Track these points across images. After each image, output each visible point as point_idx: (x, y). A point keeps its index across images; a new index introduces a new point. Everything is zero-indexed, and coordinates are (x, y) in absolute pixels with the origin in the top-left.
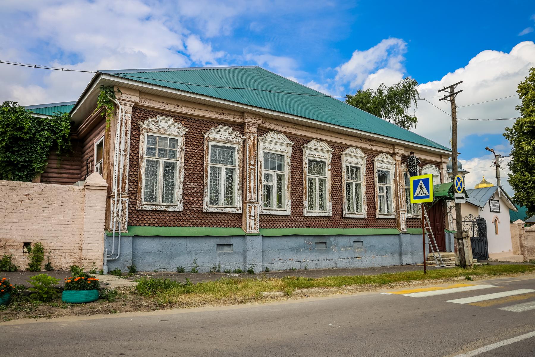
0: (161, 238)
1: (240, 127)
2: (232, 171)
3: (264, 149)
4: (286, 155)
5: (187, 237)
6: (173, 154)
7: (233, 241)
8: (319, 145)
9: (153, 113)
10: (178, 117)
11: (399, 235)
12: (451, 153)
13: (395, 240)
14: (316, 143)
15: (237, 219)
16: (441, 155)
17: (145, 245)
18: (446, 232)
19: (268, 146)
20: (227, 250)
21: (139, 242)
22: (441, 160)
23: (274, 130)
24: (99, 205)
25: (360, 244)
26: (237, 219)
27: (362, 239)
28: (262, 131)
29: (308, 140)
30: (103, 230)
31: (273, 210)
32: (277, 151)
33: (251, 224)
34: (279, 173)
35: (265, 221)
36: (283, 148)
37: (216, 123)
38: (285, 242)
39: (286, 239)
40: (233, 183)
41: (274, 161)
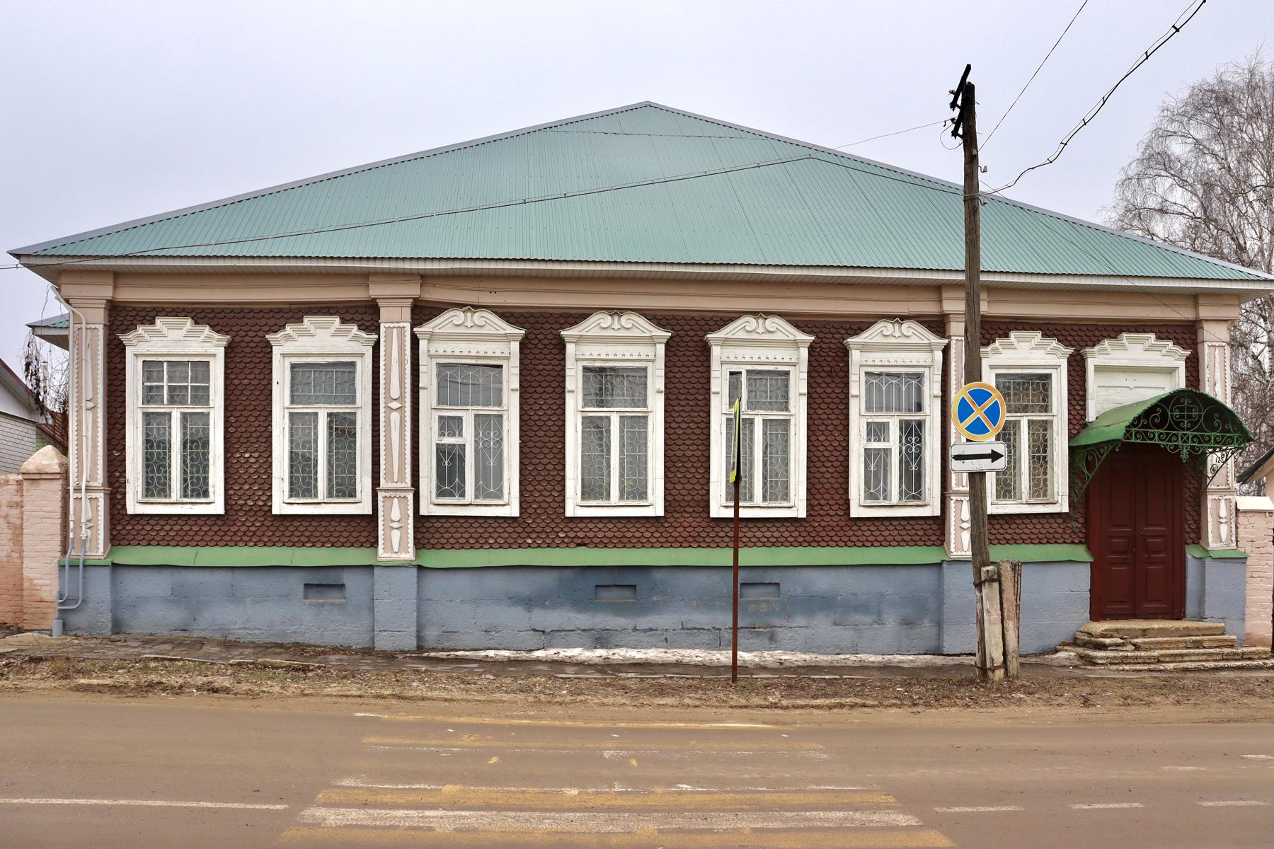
0: (175, 570)
1: (365, 316)
2: (1045, 425)
3: (992, 367)
4: (358, 361)
5: (847, 566)
6: (202, 395)
7: (347, 578)
8: (897, 334)
9: (148, 314)
10: (202, 315)
11: (940, 565)
12: (962, 277)
13: (926, 577)
14: (606, 320)
15: (364, 529)
16: (937, 289)
17: (137, 585)
18: (1191, 553)
19: (441, 347)
20: (333, 597)
21: (130, 578)
22: (1197, 313)
23: (460, 306)
24: (50, 509)
25: (627, 593)
26: (364, 529)
27: (774, 577)
28: (422, 312)
29: (860, 325)
30: (59, 554)
31: (469, 505)
32: (472, 357)
33: (396, 542)
34: (1041, 417)
35: (991, 529)
36: (1053, 360)
37: (296, 313)
38: (497, 582)
39: (866, 574)
40: (1049, 449)
41: (464, 380)
